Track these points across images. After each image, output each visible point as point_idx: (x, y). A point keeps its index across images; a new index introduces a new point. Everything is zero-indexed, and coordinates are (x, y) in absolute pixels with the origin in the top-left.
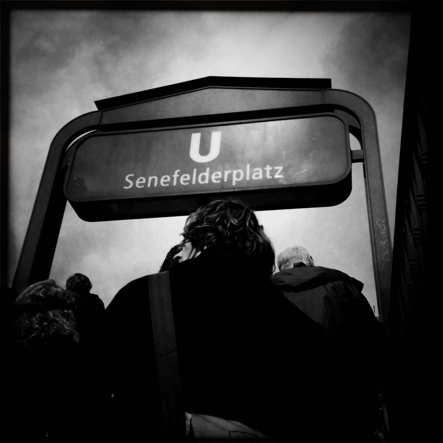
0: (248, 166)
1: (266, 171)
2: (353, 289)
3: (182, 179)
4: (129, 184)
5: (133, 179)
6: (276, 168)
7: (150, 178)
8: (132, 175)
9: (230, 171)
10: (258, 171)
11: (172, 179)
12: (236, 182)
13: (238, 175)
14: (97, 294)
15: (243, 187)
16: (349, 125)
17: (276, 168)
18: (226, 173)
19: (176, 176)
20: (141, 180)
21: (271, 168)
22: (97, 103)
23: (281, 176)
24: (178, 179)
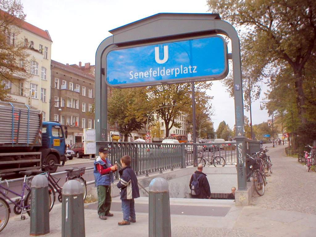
0: (181, 66)
1: (189, 68)
2: (10, 172)
3: (153, 74)
4: (131, 77)
5: (133, 74)
6: (193, 67)
7: (140, 73)
8: (132, 72)
9: (174, 69)
10: (186, 69)
11: (149, 73)
12: (177, 75)
13: (177, 72)
14: (220, 122)
15: (19, 78)
16: (109, 31)
17: (193, 67)
18: (172, 70)
19: (151, 72)
20: (136, 74)
21: (191, 67)
22: (111, 31)
23: (196, 72)
24: (152, 73)
